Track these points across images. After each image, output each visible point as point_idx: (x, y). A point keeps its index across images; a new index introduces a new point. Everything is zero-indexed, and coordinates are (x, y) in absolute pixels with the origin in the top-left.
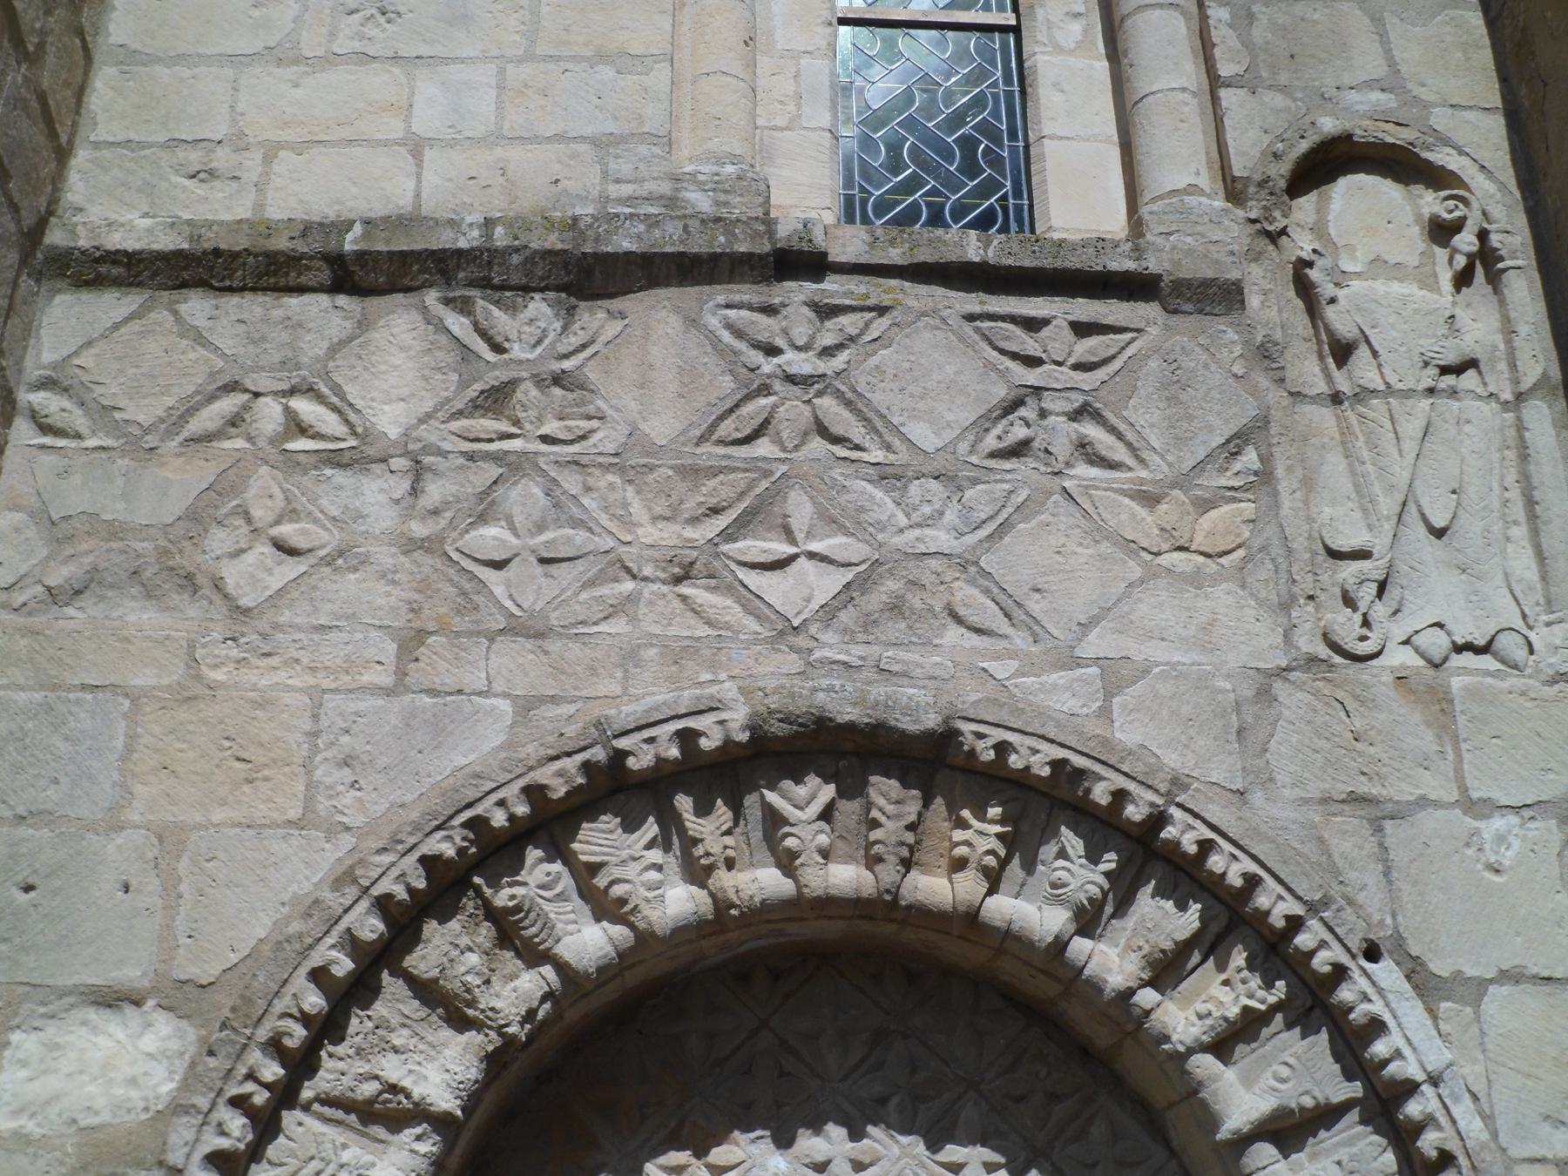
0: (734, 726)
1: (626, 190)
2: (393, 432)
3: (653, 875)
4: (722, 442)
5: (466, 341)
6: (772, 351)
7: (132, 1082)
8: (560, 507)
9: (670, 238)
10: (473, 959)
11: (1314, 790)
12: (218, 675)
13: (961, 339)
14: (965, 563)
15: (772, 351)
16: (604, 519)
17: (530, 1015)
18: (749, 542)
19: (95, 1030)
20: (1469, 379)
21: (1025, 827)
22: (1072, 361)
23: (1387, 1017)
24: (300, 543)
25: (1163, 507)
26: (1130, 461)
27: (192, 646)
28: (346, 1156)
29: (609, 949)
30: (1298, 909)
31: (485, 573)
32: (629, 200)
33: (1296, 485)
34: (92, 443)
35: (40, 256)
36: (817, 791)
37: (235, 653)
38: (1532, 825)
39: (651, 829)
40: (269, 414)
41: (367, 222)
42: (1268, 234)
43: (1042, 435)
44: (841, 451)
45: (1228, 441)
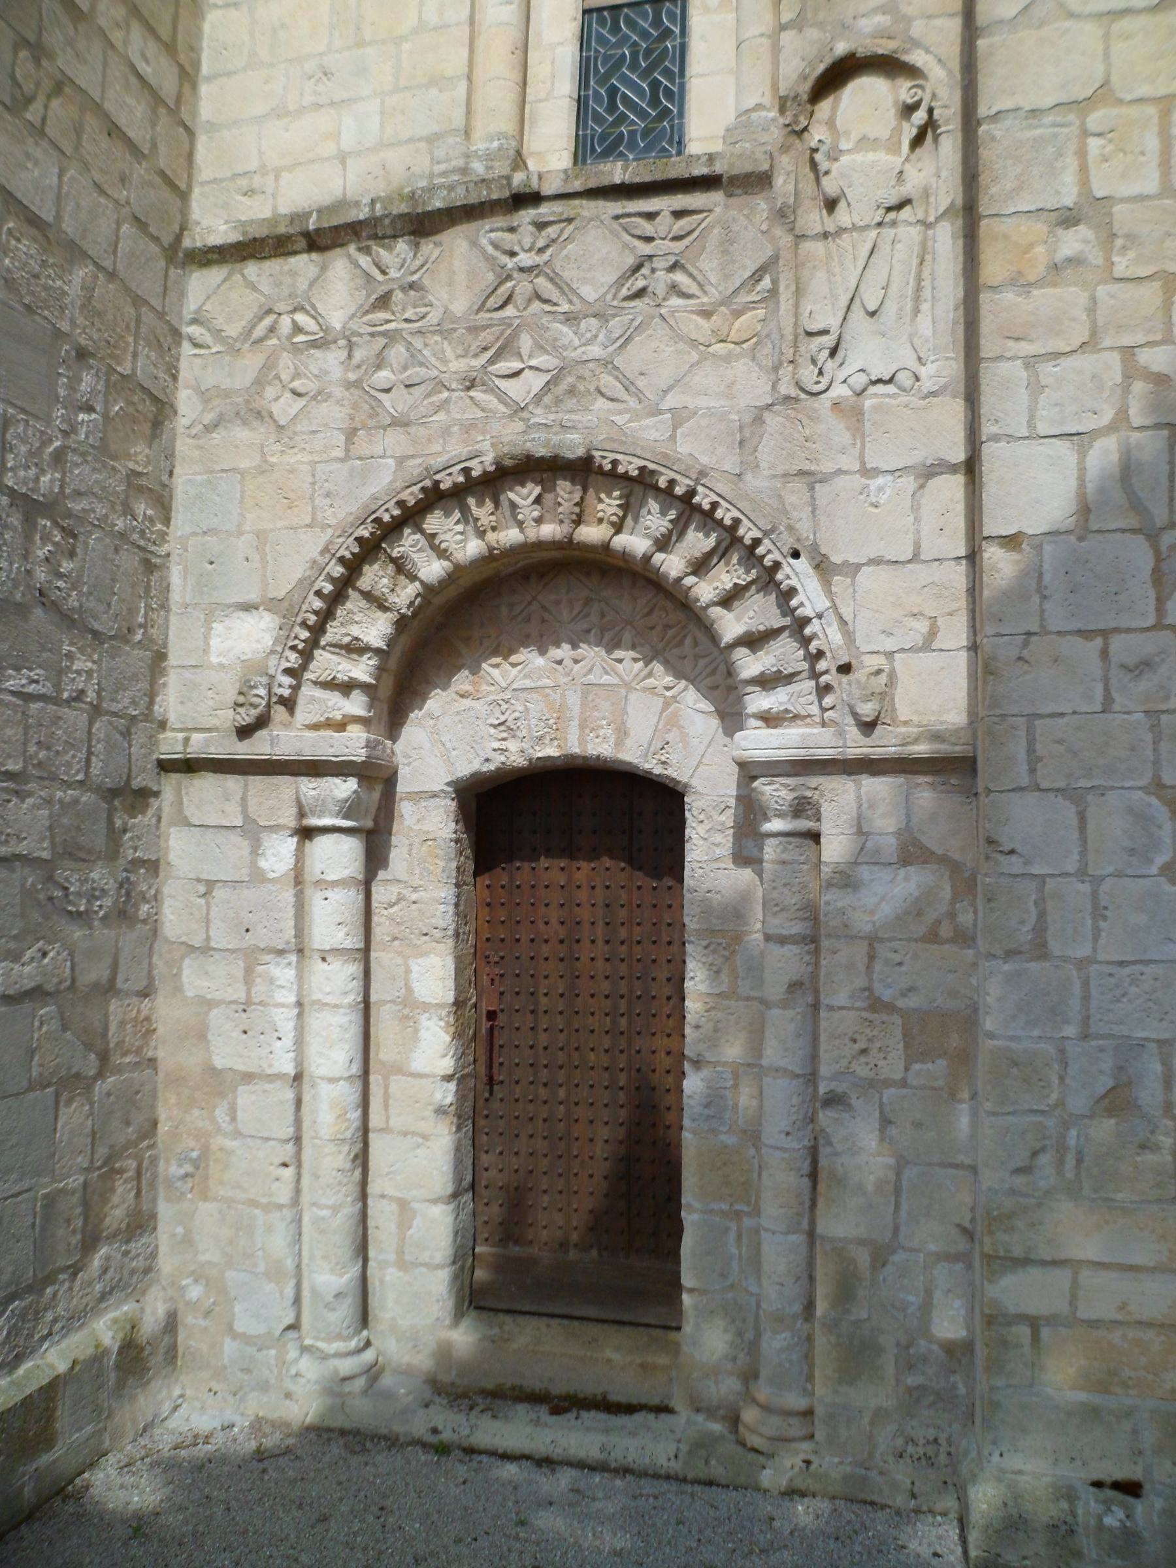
0: (487, 463)
1: (443, 167)
2: (338, 326)
3: (459, 537)
4: (489, 311)
5: (369, 271)
6: (513, 254)
7: (258, 641)
8: (414, 357)
9: (460, 197)
10: (385, 581)
11: (779, 470)
12: (273, 460)
13: (611, 232)
14: (607, 363)
15: (513, 254)
16: (433, 360)
17: (412, 603)
18: (502, 364)
19: (243, 620)
20: (906, 213)
21: (633, 500)
22: (671, 236)
23: (799, 587)
24: (301, 390)
25: (714, 318)
26: (698, 293)
27: (262, 447)
28: (340, 668)
29: (443, 573)
30: (759, 535)
31: (381, 396)
32: (444, 174)
33: (790, 296)
34: (214, 350)
35: (181, 255)
36: (533, 490)
37: (280, 448)
38: (900, 480)
39: (457, 515)
40: (285, 323)
41: (319, 211)
42: (795, 132)
43: (653, 284)
44: (547, 308)
45: (754, 274)
